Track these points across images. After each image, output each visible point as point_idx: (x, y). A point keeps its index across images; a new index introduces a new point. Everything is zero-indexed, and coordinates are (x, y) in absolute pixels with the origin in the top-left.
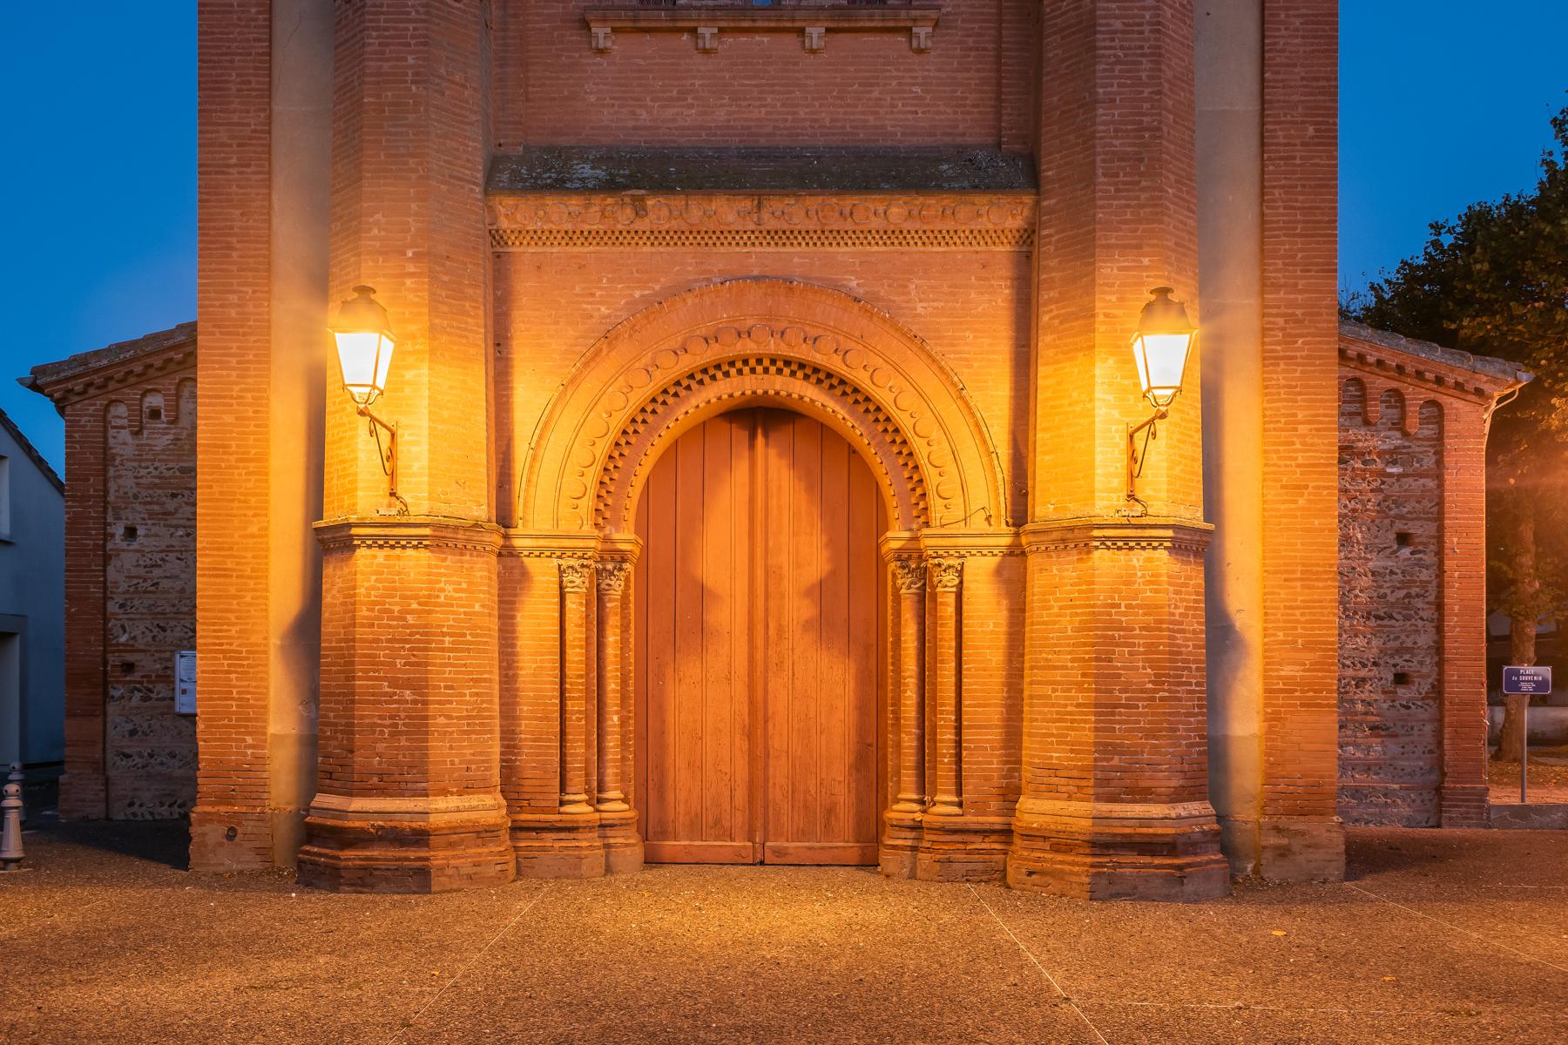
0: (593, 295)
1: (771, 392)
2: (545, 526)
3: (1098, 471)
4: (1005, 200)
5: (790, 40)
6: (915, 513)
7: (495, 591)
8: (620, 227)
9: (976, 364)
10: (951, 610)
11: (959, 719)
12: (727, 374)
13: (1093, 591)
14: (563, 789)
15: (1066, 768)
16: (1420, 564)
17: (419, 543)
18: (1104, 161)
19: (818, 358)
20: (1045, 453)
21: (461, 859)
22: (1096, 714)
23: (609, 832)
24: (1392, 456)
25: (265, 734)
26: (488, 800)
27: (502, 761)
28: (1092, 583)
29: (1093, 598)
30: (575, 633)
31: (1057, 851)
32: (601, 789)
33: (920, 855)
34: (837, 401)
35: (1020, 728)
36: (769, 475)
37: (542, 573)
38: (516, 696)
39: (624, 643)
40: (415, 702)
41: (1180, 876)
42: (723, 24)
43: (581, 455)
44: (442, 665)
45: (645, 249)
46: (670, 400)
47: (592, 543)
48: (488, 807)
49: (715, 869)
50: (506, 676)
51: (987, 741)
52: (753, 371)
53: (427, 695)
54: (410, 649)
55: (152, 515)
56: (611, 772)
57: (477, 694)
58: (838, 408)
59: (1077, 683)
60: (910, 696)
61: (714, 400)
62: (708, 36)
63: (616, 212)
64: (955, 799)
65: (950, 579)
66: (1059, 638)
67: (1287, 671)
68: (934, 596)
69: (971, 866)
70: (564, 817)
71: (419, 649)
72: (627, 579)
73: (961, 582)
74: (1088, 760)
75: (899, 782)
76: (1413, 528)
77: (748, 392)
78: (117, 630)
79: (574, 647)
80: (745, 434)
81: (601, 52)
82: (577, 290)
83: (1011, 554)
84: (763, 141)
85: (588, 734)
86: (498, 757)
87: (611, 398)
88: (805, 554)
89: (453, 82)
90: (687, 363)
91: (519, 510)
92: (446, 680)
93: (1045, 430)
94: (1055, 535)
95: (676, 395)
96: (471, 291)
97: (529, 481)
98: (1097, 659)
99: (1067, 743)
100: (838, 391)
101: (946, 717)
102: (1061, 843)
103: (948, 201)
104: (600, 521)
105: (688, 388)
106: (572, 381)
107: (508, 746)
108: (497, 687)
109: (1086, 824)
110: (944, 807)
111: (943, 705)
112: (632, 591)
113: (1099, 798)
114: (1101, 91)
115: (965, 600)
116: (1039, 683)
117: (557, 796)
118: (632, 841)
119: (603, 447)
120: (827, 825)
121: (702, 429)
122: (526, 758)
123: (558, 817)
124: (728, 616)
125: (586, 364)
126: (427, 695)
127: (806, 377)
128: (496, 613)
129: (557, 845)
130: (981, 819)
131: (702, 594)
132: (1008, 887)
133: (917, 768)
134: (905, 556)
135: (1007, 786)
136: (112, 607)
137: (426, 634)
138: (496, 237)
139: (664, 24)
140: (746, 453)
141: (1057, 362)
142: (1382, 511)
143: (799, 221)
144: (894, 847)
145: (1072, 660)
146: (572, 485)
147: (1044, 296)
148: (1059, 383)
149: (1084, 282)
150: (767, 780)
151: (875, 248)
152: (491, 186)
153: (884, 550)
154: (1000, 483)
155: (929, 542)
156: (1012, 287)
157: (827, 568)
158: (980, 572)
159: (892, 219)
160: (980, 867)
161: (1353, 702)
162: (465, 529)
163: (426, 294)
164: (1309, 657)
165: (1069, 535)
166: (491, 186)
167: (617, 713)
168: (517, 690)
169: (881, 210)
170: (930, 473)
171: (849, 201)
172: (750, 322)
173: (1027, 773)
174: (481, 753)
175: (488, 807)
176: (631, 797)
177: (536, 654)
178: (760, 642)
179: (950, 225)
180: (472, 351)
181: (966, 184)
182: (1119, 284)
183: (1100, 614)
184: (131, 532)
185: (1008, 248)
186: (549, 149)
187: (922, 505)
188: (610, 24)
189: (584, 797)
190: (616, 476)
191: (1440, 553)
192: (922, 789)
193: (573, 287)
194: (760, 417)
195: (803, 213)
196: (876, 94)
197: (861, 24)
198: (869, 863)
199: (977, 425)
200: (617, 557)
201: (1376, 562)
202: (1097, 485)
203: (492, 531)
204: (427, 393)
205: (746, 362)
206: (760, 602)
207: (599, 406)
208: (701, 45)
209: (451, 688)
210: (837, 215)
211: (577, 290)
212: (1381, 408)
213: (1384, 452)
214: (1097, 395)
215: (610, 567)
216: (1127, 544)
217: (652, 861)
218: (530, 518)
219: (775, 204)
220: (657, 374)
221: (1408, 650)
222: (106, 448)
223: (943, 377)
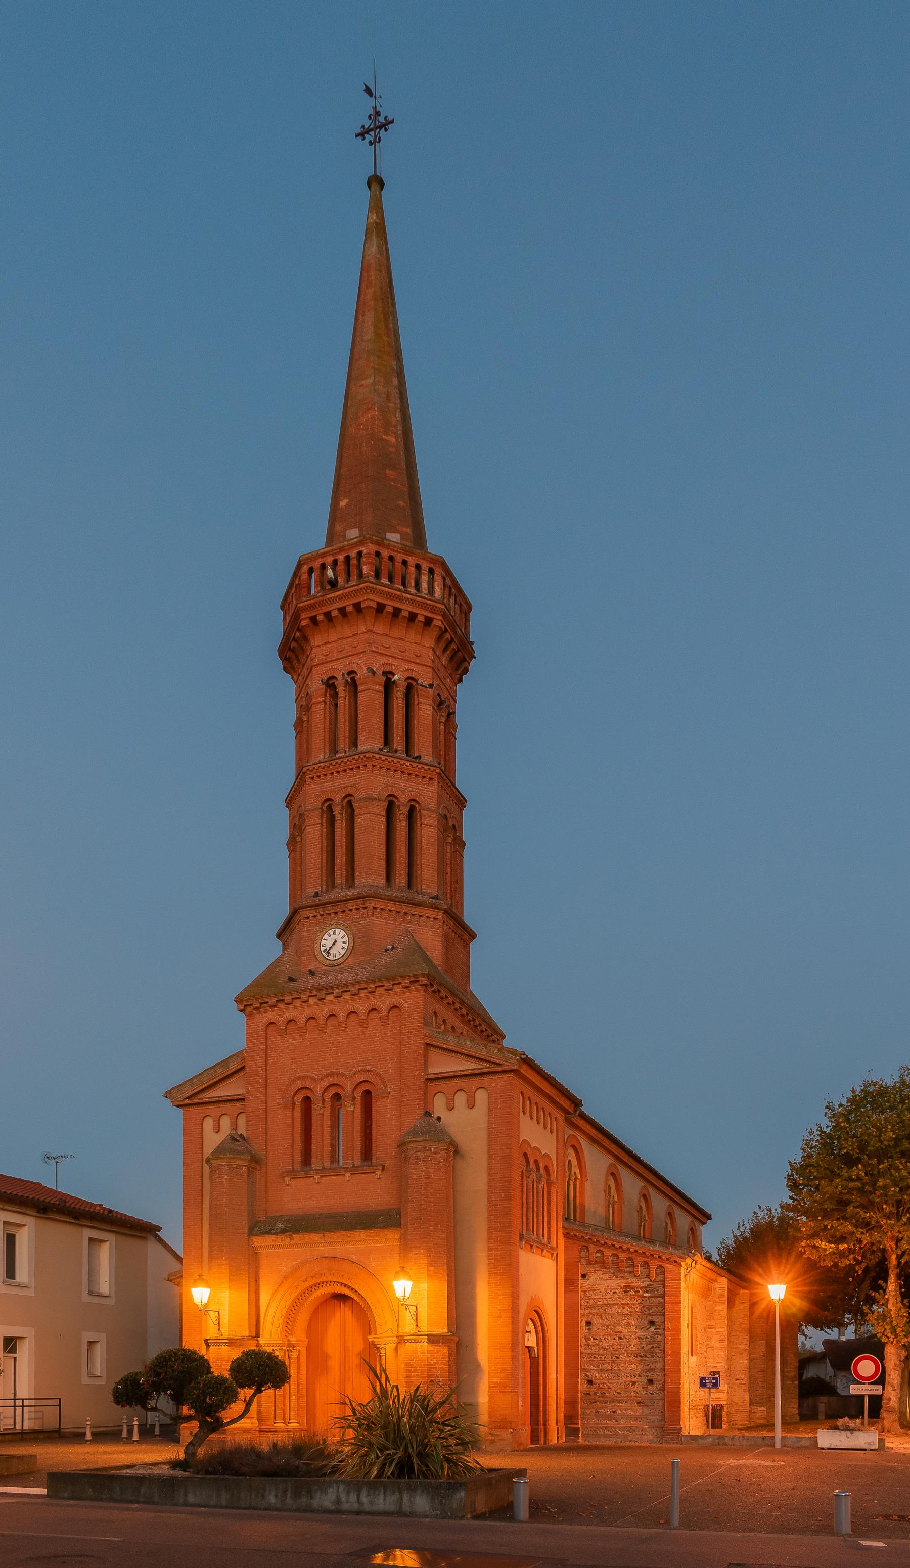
16: (657, 1334)
24: (646, 1289)
67: (495, 1380)
76: (655, 1319)
84: (334, 1211)
90: (307, 1284)
124: (334, 1363)
131: (326, 1356)
142: (642, 1312)
161: (630, 1392)
164: (503, 1375)
166: (251, 1232)
171: (349, 1233)
201: (640, 1333)
213: (645, 1287)
216: (415, 1341)
219: (328, 1235)
221: (653, 1370)
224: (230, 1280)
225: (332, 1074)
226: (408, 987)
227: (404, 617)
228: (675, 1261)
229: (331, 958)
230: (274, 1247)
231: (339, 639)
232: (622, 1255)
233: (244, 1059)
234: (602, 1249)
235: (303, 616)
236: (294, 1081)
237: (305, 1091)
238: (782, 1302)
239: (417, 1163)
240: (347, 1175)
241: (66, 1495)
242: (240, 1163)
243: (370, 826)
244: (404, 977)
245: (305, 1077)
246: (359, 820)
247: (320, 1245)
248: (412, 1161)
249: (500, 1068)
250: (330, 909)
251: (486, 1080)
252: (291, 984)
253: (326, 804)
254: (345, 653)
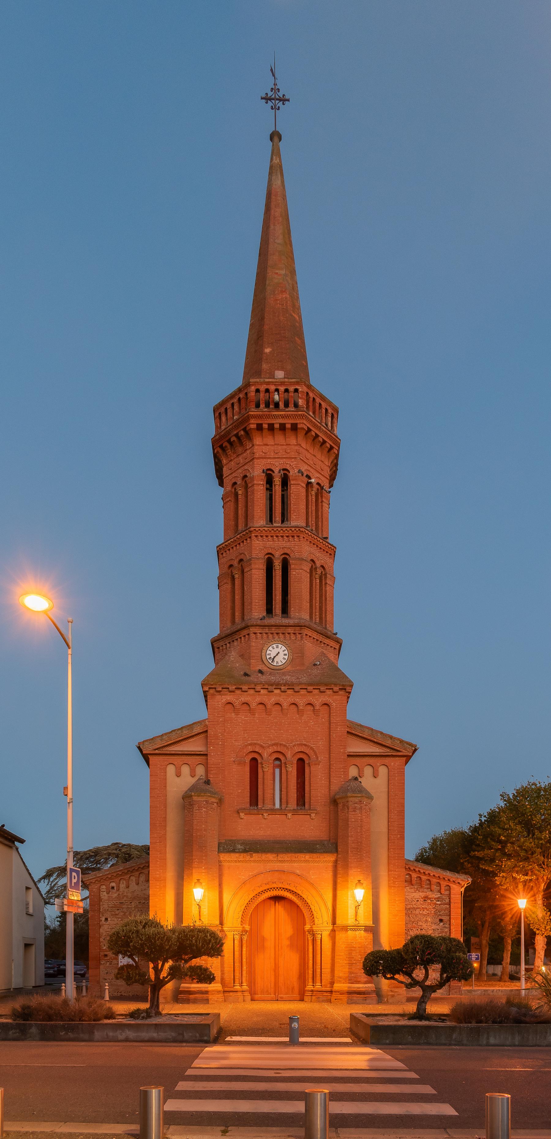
4: (330, 855)
10: (319, 943)
16: (445, 927)
24: (438, 899)
25: (469, 952)
41: (365, 999)
55: (112, 915)
56: (244, 979)
60: (311, 962)
63: (247, 857)
65: (319, 936)
74: (347, 975)
76: (443, 918)
78: (103, 946)
80: (273, 902)
84: (278, 839)
87: (244, 898)
88: (287, 929)
91: (225, 921)
101: (318, 967)
102: (342, 993)
103: (318, 855)
110: (318, 986)
120: (292, 992)
124: (270, 944)
131: (263, 939)
136: (101, 940)
138: (220, 862)
142: (435, 914)
143: (286, 858)
149: (346, 874)
152: (219, 852)
158: (326, 934)
166: (219, 852)
170: (315, 913)
171: (297, 855)
182: (355, 874)
184: (106, 919)
186: (230, 840)
191: (450, 924)
194: (277, 899)
212: (435, 887)
213: (437, 898)
216: (355, 930)
217: (252, 1000)
219: (281, 855)
222: (100, 897)
225: (276, 744)
226: (233, 692)
227: (320, 441)
228: (459, 883)
229: (275, 664)
231: (276, 444)
232: (424, 878)
233: (206, 726)
234: (410, 873)
235: (252, 421)
236: (246, 746)
237: (253, 754)
238: (525, 910)
239: (354, 811)
240: (289, 815)
241: (388, 1041)
242: (214, 800)
243: (257, 575)
244: (335, 685)
245: (255, 744)
246: (294, 573)
247: (271, 862)
248: (350, 810)
249: (400, 754)
250: (274, 630)
251: (387, 760)
252: (247, 678)
253: (283, 556)
254: (280, 455)
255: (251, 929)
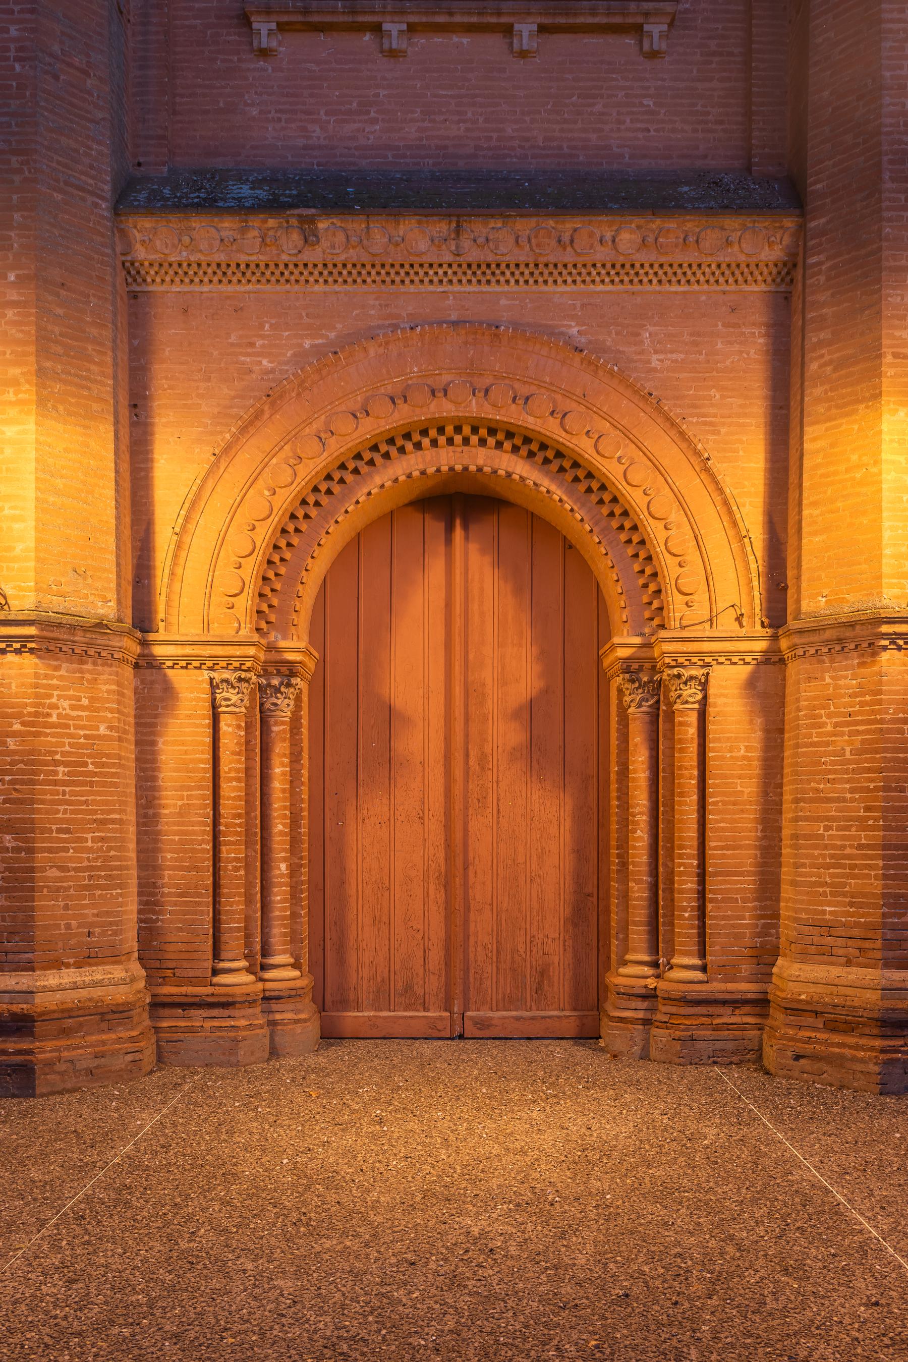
0: (252, 345)
1: (473, 468)
2: (193, 631)
3: (887, 551)
5: (494, 43)
6: (647, 614)
7: (130, 710)
8: (285, 258)
9: (723, 430)
11: (702, 865)
12: (418, 446)
13: (880, 702)
14: (216, 955)
15: (844, 925)
17: (22, 646)
18: (891, 162)
19: (530, 422)
20: (815, 533)
21: (81, 1049)
22: (884, 857)
23: (274, 1006)
26: (118, 972)
27: (140, 921)
28: (880, 692)
29: (880, 712)
30: (231, 763)
31: (834, 1030)
32: (265, 953)
33: (655, 1031)
34: (552, 479)
35: (778, 875)
36: (468, 574)
37: (190, 687)
38: (156, 841)
39: (294, 777)
40: (17, 850)
42: (413, 19)
43: (238, 542)
44: (53, 802)
45: (316, 288)
46: (349, 478)
47: (252, 651)
48: (119, 981)
49: (405, 1046)
50: (145, 816)
51: (738, 891)
52: (450, 441)
53: (33, 840)
54: (11, 782)
56: (278, 931)
57: (102, 839)
58: (553, 488)
59: (858, 819)
60: (641, 836)
61: (402, 478)
62: (395, 34)
64: (697, 962)
65: (692, 693)
66: (833, 763)
68: (670, 715)
69: (719, 1045)
70: (217, 990)
71: (23, 782)
72: (298, 699)
73: (705, 697)
74: (874, 916)
75: (626, 938)
77: (445, 468)
79: (231, 780)
81: (264, 53)
82: (233, 339)
83: (767, 662)
85: (249, 886)
86: (134, 917)
88: (512, 668)
89: (70, 65)
90: (369, 429)
92: (61, 821)
93: (814, 504)
94: (828, 634)
95: (356, 471)
96: (94, 331)
97: (172, 574)
98: (885, 789)
99: (844, 895)
100: (554, 467)
102: (839, 1020)
103: (692, 224)
104: (263, 625)
105: (371, 463)
106: (227, 450)
107: (147, 903)
108: (132, 829)
109: (873, 996)
110: (684, 971)
111: (682, 847)
112: (305, 713)
113: (888, 964)
114: (887, 74)
115: (710, 718)
116: (807, 819)
117: (208, 964)
118: (303, 1016)
119: (264, 533)
120: (539, 991)
121: (388, 520)
122: (170, 917)
123: (209, 990)
124: (422, 742)
125: (243, 430)
126: (33, 840)
127: (515, 449)
128: (131, 737)
129: (208, 1024)
130: (730, 986)
131: (389, 716)
132: (767, 1073)
133: (649, 924)
134: (635, 666)
135: (762, 947)
137: (32, 763)
138: (132, 272)
139: (341, 19)
140: (442, 549)
141: (830, 419)
143: (507, 251)
144: (622, 1020)
145: (852, 790)
146: (227, 580)
147: (812, 339)
148: (832, 445)
150: (467, 937)
151: (601, 288)
153: (606, 663)
154: (754, 574)
155: (666, 647)
156: (767, 335)
157: (538, 684)
158: (729, 683)
159: (622, 247)
160: (730, 1046)
162: (85, 629)
163: (33, 329)
165: (849, 633)
167: (285, 860)
168: (159, 833)
169: (608, 235)
171: (569, 224)
172: (446, 378)
173: (787, 931)
174: (108, 914)
175: (119, 981)
176: (305, 960)
177: (182, 788)
178: (458, 773)
179: (692, 256)
180: (96, 407)
181: (713, 204)
183: (889, 731)
185: (763, 287)
187: (656, 604)
188: (275, 18)
189: (243, 963)
190: (282, 570)
192: (654, 948)
193: (228, 335)
194: (459, 503)
195: (512, 240)
196: (598, 108)
197: (581, 20)
198: (588, 1036)
199: (726, 503)
200: (284, 670)
202: (886, 570)
203: (121, 633)
204: (33, 455)
205: (441, 430)
206: (459, 726)
207: (260, 483)
208: (386, 46)
209: (67, 831)
210: (554, 243)
211: (233, 339)
214: (884, 456)
215: (275, 682)
217: (330, 1036)
218: (173, 619)
219: (478, 228)
220: (332, 442)
223: (684, 446)
224: (41, 372)
230: (222, 271)
255: (322, 663)
